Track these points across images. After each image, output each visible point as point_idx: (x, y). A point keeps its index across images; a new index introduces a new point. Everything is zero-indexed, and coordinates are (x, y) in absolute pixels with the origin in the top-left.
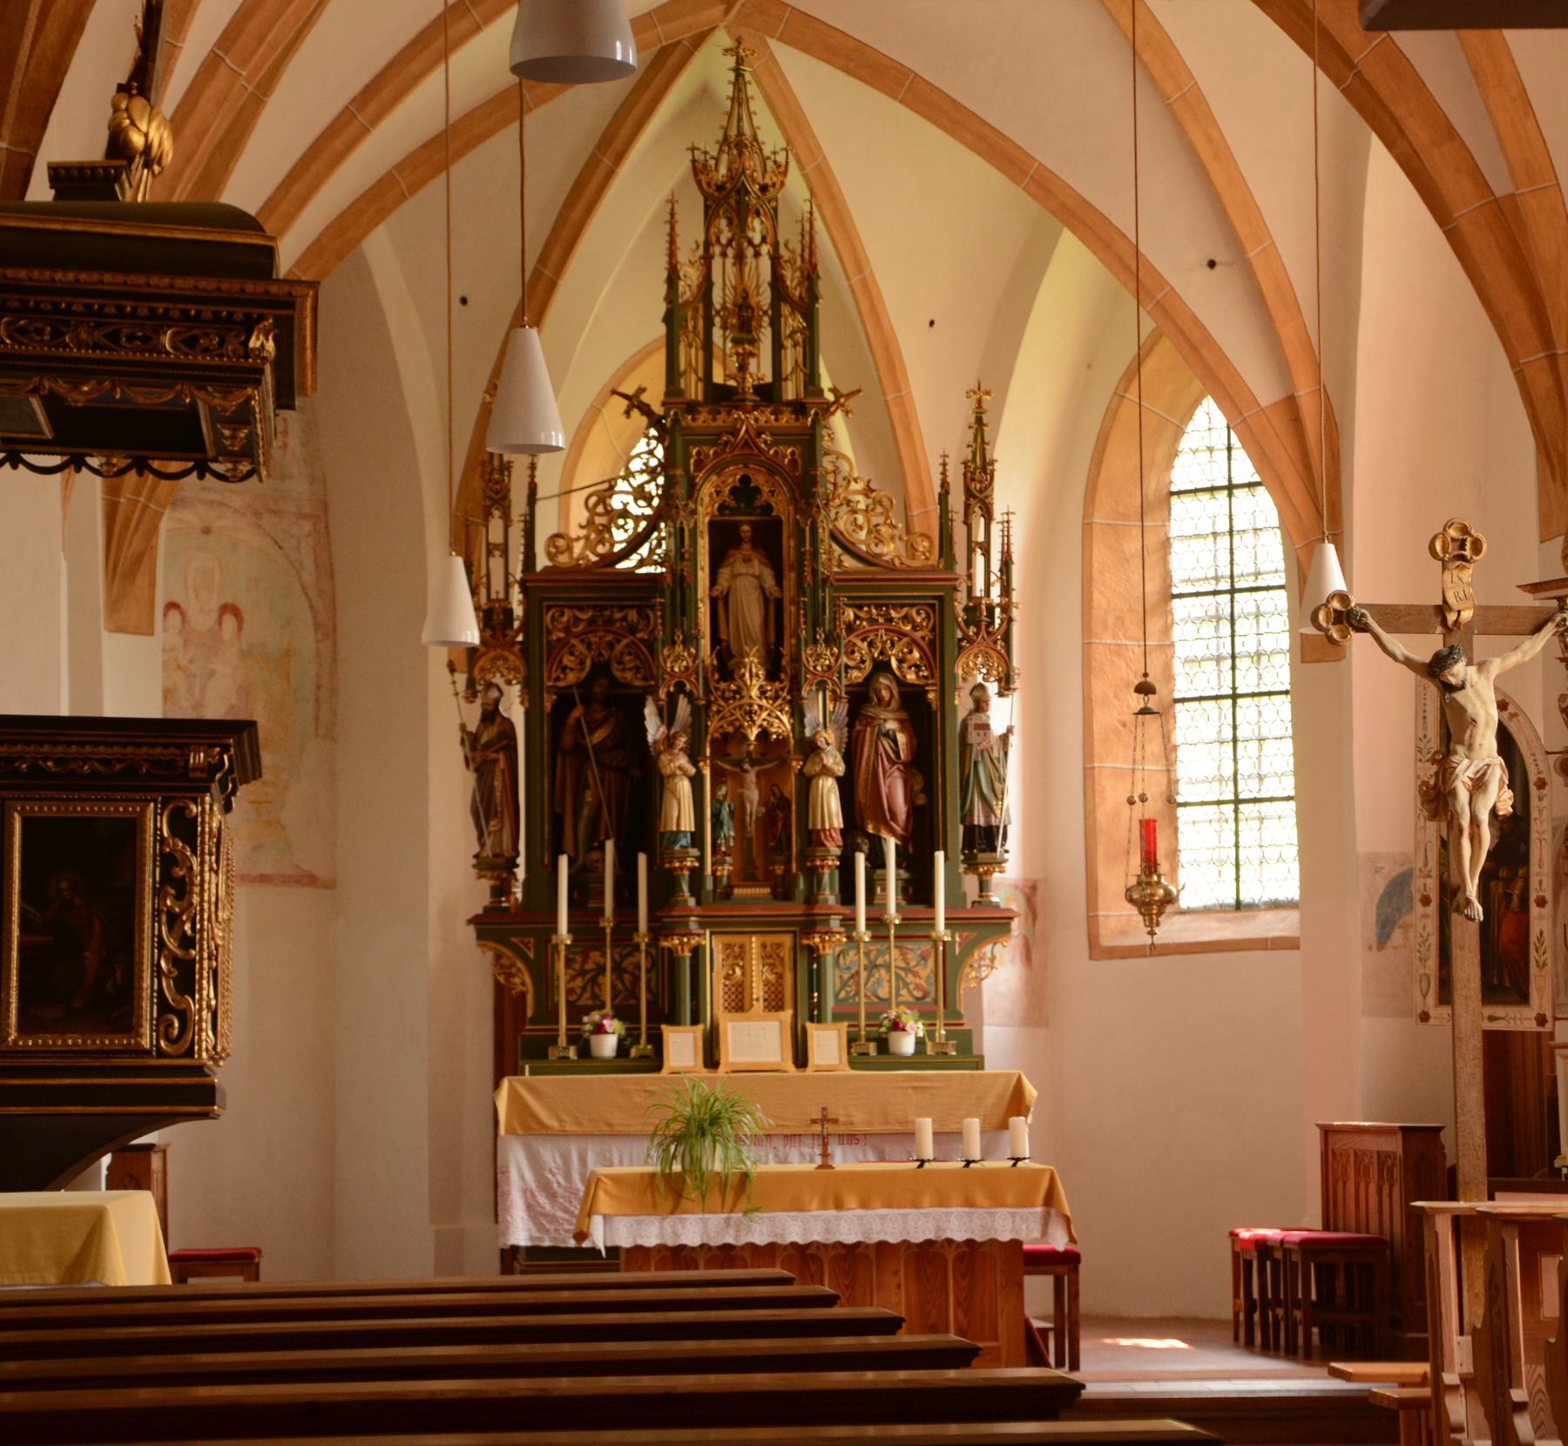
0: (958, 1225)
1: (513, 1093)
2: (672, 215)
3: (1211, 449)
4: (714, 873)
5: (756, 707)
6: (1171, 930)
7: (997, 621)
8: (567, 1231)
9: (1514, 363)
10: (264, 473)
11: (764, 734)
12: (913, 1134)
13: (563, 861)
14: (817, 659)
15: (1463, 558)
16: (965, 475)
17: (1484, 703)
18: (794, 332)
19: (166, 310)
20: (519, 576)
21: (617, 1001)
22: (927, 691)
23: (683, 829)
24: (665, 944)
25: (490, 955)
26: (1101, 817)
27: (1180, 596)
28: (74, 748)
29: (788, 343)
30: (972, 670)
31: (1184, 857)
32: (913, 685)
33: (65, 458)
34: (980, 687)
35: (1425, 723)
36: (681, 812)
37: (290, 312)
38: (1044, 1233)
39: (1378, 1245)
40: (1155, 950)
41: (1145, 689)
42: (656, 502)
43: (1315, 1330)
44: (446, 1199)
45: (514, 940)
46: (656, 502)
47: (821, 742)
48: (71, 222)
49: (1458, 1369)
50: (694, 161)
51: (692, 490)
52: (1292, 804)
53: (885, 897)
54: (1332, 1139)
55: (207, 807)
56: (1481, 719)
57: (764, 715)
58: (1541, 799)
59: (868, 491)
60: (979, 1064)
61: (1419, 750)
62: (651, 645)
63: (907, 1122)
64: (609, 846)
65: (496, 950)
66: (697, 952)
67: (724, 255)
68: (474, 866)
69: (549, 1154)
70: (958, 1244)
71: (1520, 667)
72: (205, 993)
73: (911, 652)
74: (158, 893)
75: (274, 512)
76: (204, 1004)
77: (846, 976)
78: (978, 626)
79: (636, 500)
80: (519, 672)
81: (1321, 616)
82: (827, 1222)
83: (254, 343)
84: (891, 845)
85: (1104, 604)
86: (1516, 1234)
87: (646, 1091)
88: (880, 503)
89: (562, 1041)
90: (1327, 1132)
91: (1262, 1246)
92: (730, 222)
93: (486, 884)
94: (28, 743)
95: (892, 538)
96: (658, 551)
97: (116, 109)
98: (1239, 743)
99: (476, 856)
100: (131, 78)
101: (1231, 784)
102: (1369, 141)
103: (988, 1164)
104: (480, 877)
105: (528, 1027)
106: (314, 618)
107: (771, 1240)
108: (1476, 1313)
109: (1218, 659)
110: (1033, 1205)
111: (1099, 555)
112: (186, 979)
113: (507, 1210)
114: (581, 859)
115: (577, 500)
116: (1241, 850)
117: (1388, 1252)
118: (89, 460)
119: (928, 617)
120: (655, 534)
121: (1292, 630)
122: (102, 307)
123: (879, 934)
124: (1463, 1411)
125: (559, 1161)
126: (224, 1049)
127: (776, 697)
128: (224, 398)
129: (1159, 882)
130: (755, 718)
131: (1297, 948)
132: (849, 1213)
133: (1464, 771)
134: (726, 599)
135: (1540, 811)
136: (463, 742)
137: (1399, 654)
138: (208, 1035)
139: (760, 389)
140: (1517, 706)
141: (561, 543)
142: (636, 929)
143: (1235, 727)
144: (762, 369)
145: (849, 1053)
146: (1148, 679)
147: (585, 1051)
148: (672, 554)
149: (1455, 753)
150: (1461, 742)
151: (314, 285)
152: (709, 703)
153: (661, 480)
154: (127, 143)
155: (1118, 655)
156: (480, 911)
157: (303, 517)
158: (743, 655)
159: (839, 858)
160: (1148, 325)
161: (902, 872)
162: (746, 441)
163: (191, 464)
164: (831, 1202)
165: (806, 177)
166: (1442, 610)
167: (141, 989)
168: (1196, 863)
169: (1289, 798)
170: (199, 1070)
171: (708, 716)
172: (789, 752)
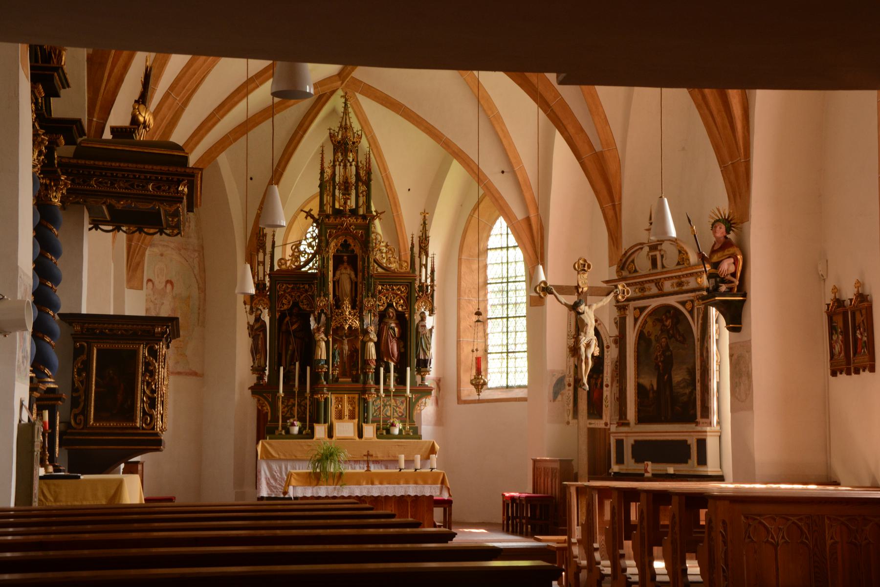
0: (412, 490)
1: (263, 445)
2: (323, 151)
3: (501, 234)
4: (332, 373)
5: (348, 318)
6: (485, 395)
7: (429, 291)
8: (281, 492)
9: (601, 207)
10: (183, 234)
11: (350, 327)
12: (398, 461)
13: (282, 369)
14: (369, 302)
15: (584, 270)
16: (419, 241)
17: (590, 319)
18: (363, 192)
19: (150, 177)
20: (268, 272)
21: (299, 415)
22: (405, 314)
23: (322, 358)
24: (316, 397)
25: (256, 400)
26: (463, 357)
27: (490, 284)
28: (115, 326)
29: (361, 195)
30: (421, 307)
31: (489, 371)
32: (401, 312)
33: (114, 227)
34: (423, 313)
35: (570, 326)
36: (322, 353)
37: (193, 179)
38: (441, 493)
39: (550, 498)
40: (480, 401)
41: (478, 313)
42: (315, 248)
43: (529, 526)
44: (239, 482)
45: (264, 395)
46: (315, 248)
47: (370, 331)
48: (117, 146)
49: (576, 537)
50: (330, 133)
51: (328, 244)
52: (526, 353)
53: (390, 383)
54: (536, 463)
55: (161, 346)
56: (589, 324)
57: (350, 321)
58: (608, 352)
59: (387, 246)
60: (420, 437)
61: (568, 335)
62: (313, 296)
63: (395, 457)
64: (297, 364)
65: (258, 398)
66: (326, 399)
67: (340, 165)
68: (251, 370)
69: (275, 466)
70: (412, 497)
71: (602, 307)
72: (159, 409)
73: (400, 300)
74: (144, 375)
75: (185, 249)
76: (159, 412)
77: (376, 408)
78: (423, 292)
79: (308, 247)
80: (268, 305)
81: (538, 289)
82: (368, 489)
83: (180, 189)
84: (392, 365)
85: (465, 286)
86: (597, 492)
87: (308, 445)
88: (391, 250)
89: (280, 428)
90: (535, 461)
91: (513, 498)
92: (342, 154)
93: (255, 376)
94: (99, 324)
95: (395, 262)
96: (316, 265)
97: (134, 108)
98: (509, 333)
99: (252, 367)
100: (139, 99)
101: (506, 347)
102: (555, 131)
103: (423, 470)
104: (253, 374)
105: (269, 424)
106: (198, 285)
107: (349, 495)
108: (583, 519)
109: (502, 305)
110: (437, 484)
111: (464, 269)
112: (153, 404)
113: (260, 484)
114: (288, 368)
115: (288, 247)
116: (509, 369)
117: (554, 501)
118: (122, 228)
119: (406, 289)
120: (315, 259)
121: (527, 295)
122: (128, 175)
123: (388, 394)
124: (578, 551)
125: (278, 468)
126: (165, 428)
127: (355, 315)
128: (170, 207)
129: (481, 378)
130: (347, 322)
131: (526, 401)
132: (376, 486)
133: (583, 341)
134: (338, 282)
135: (607, 356)
136: (248, 328)
137: (563, 302)
138: (160, 423)
139: (351, 211)
140: (601, 321)
141: (283, 261)
142: (306, 391)
143: (507, 328)
144: (352, 203)
145: (377, 434)
146: (480, 310)
147: (288, 432)
148: (320, 266)
149: (581, 335)
150: (583, 332)
151: (201, 170)
152: (332, 316)
153: (317, 241)
154: (138, 120)
155: (469, 303)
156: (253, 385)
157: (195, 251)
158: (344, 300)
159: (374, 369)
160: (481, 192)
161: (395, 374)
162: (346, 228)
163: (157, 230)
164: (370, 483)
165: (368, 140)
166: (577, 287)
167: (137, 407)
168: (494, 373)
169: (525, 352)
170: (157, 434)
171: (331, 320)
172: (358, 333)
